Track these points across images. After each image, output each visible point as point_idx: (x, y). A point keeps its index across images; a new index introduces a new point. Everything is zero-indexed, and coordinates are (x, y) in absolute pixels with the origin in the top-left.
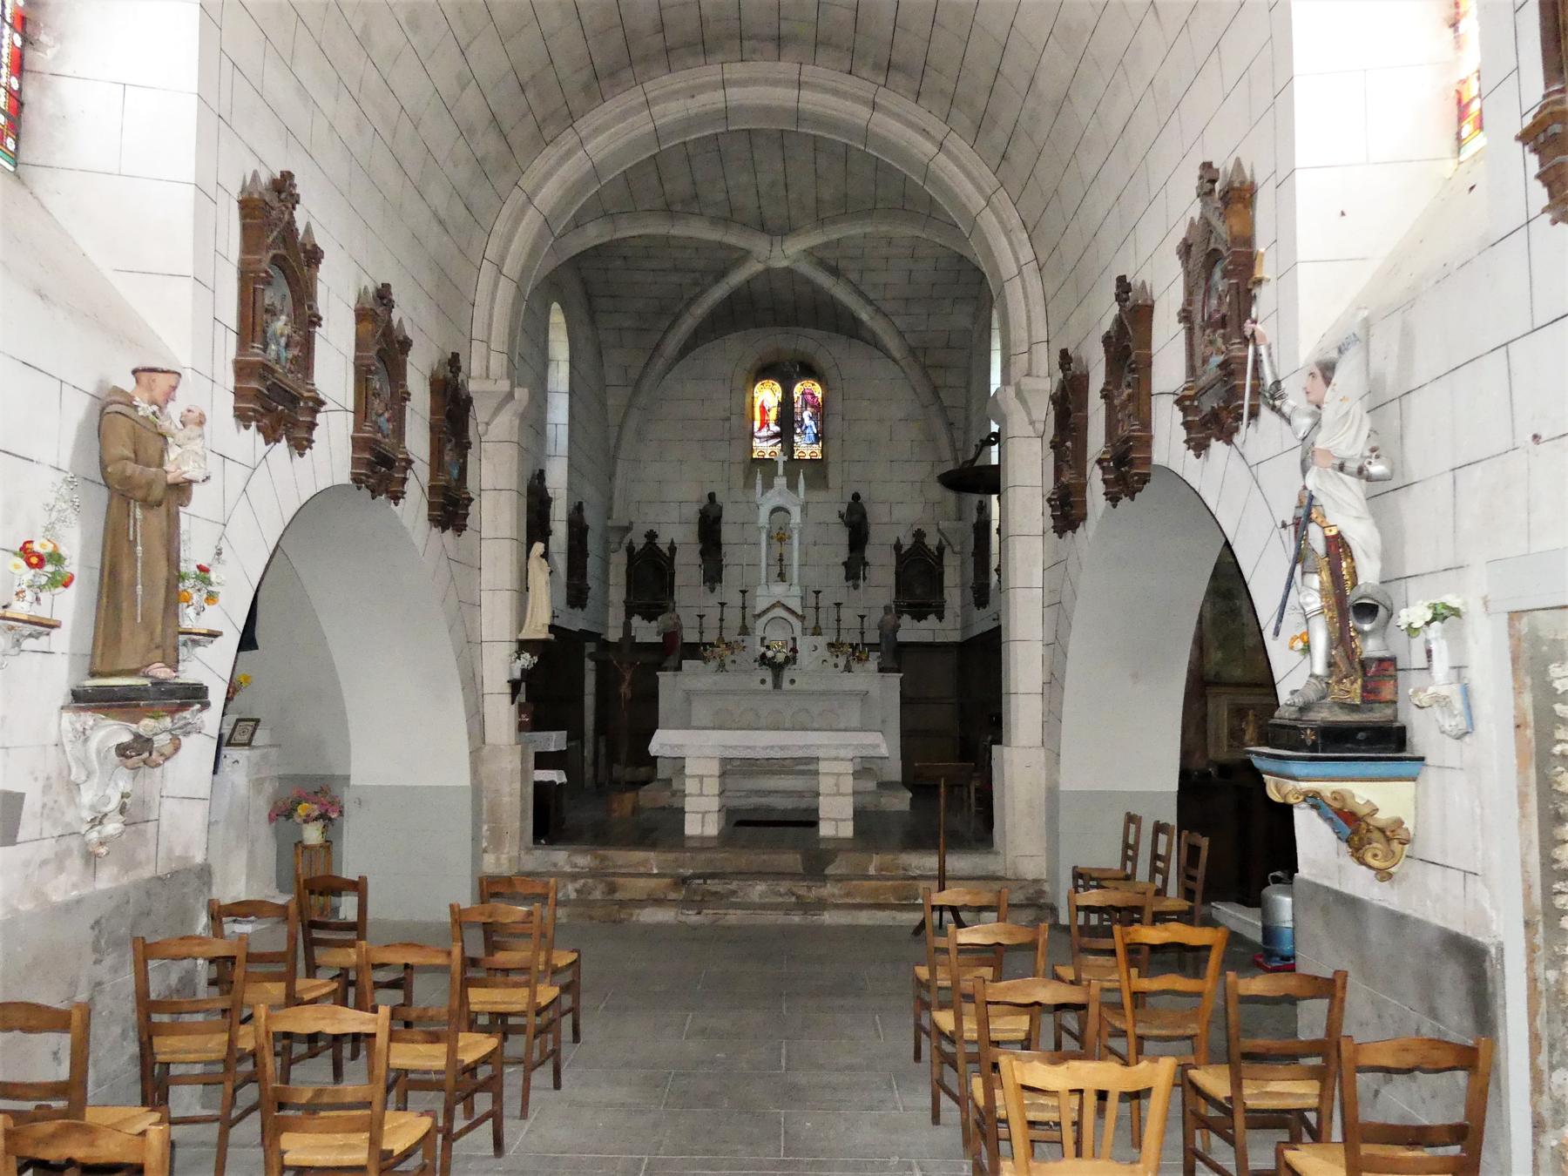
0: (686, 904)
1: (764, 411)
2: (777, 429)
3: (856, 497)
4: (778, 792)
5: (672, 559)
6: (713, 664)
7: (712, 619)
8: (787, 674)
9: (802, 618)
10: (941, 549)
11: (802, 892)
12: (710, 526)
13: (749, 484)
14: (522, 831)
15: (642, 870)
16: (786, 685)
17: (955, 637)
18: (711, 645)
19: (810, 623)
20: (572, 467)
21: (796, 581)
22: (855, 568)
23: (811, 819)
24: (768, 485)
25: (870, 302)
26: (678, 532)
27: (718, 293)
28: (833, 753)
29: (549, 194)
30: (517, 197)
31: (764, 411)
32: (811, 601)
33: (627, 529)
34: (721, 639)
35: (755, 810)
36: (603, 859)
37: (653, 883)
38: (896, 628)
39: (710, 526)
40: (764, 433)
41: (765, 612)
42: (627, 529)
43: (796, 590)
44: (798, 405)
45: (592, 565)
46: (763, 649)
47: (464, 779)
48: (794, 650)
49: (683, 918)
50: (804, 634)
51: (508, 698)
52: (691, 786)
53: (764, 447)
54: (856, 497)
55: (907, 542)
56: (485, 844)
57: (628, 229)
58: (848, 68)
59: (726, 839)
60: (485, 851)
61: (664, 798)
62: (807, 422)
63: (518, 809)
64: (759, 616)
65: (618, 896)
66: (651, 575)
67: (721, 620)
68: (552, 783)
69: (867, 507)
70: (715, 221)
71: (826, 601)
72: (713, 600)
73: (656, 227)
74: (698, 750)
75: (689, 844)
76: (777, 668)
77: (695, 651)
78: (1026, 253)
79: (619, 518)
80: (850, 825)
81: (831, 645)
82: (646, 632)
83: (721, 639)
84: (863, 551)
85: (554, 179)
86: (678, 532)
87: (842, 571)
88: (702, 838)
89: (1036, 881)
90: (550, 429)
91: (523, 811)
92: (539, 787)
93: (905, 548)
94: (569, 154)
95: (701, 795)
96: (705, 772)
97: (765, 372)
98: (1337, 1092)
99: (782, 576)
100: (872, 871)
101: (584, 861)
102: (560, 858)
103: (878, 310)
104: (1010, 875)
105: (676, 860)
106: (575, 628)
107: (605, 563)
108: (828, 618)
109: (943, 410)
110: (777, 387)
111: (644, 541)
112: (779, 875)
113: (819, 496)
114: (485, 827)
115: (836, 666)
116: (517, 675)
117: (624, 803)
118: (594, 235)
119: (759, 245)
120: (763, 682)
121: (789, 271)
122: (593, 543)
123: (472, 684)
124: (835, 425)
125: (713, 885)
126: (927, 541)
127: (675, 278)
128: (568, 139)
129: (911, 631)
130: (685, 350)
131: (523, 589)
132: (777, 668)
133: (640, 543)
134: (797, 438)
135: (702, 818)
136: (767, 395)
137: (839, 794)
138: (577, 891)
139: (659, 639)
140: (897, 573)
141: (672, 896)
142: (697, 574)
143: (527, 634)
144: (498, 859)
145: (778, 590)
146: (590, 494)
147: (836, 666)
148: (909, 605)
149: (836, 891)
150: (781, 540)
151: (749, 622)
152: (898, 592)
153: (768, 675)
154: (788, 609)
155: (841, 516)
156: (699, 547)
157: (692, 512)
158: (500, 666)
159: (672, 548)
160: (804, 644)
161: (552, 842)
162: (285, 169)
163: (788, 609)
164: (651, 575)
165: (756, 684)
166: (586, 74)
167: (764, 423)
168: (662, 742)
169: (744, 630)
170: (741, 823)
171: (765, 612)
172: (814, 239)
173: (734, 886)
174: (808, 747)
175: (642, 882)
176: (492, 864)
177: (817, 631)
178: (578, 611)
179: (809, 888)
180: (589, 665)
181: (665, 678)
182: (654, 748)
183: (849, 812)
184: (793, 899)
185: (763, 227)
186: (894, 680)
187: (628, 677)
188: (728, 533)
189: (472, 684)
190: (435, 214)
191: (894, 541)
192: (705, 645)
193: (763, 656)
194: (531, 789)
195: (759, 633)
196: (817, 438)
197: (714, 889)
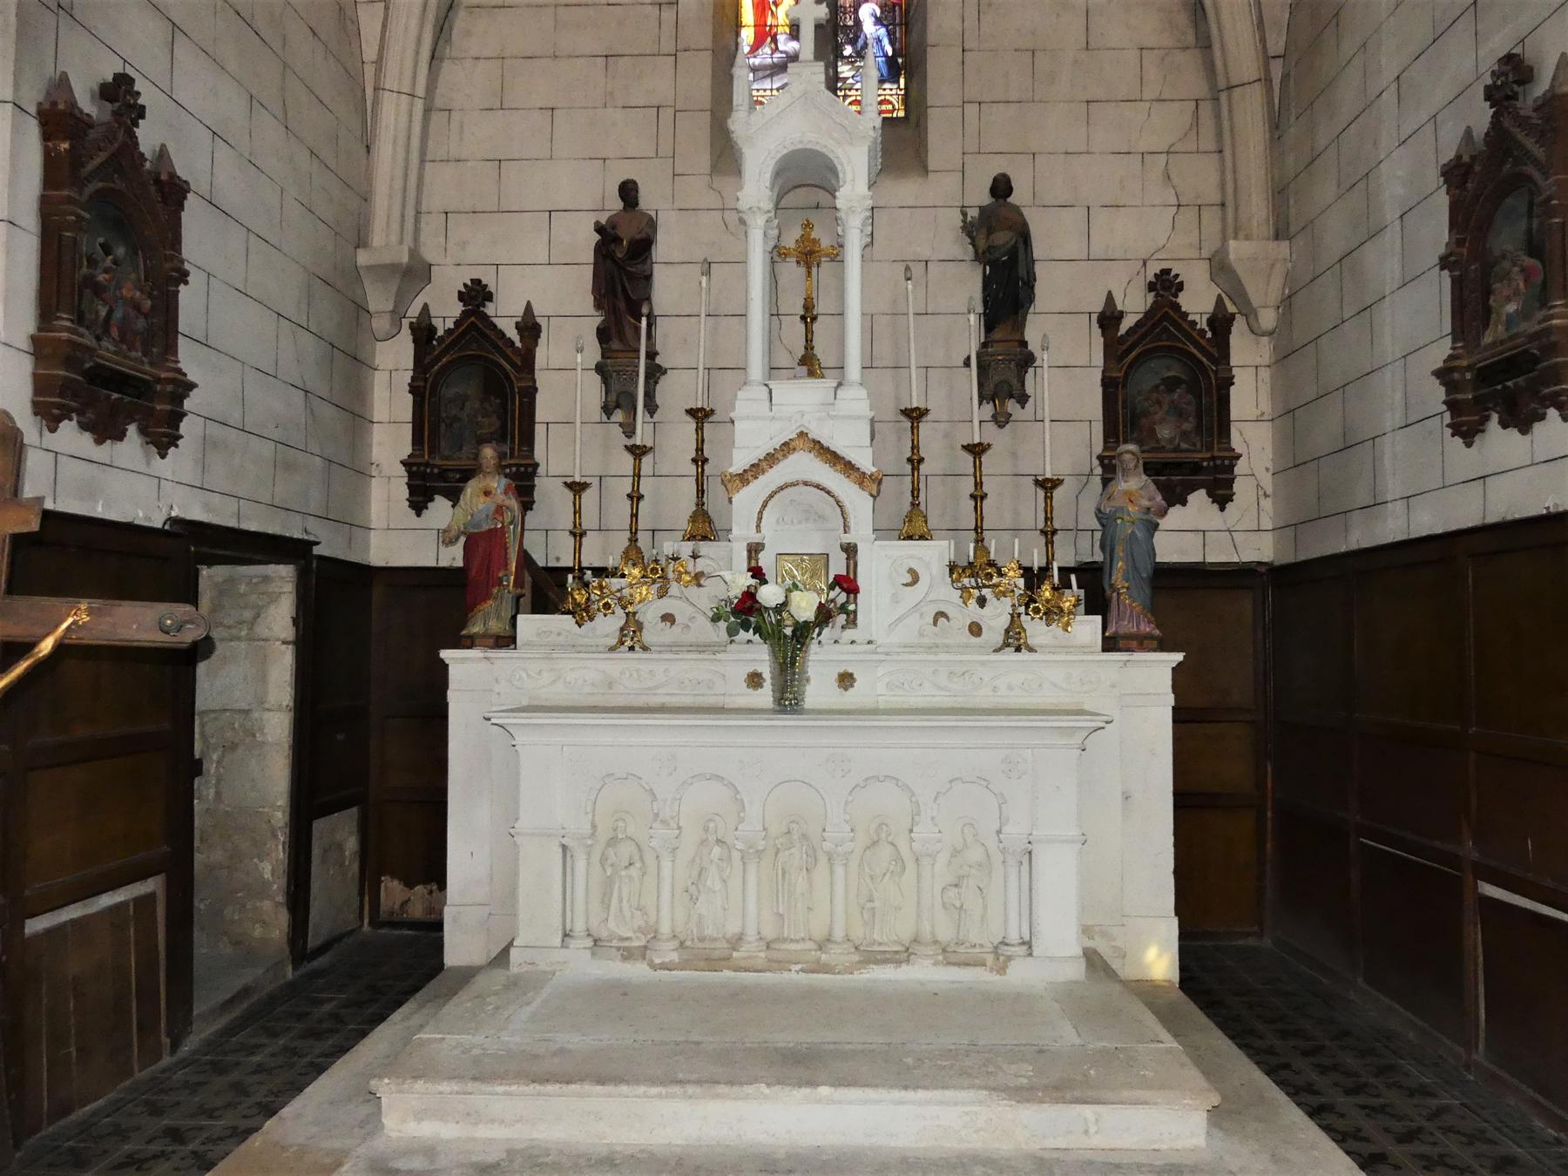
3: (1001, 187)
5: (526, 362)
6: (607, 626)
8: (822, 659)
10: (1221, 323)
12: (622, 265)
16: (818, 688)
17: (1261, 549)
22: (1003, 374)
26: (548, 286)
34: (633, 553)
39: (622, 265)
41: (756, 470)
43: (856, 401)
48: (847, 584)
50: (880, 532)
54: (1001, 187)
55: (1135, 305)
62: (870, 28)
64: (745, 478)
66: (475, 386)
76: (791, 644)
77: (548, 590)
79: (386, 242)
84: (1020, 326)
86: (548, 286)
93: (1127, 323)
98: (1241, 942)
99: (809, 364)
108: (946, 499)
111: (457, 309)
113: (906, 190)
115: (975, 629)
126: (1186, 301)
129: (1191, 533)
133: (447, 313)
139: (453, 556)
140: (1108, 384)
142: (592, 390)
145: (802, 401)
147: (975, 629)
150: (809, 255)
151: (713, 503)
153: (760, 656)
154: (832, 457)
159: (530, 328)
160: (881, 564)
162: (475, 277)
163: (832, 457)
164: (475, 386)
169: (704, 527)
171: (756, 470)
177: (913, 528)
186: (1155, 672)
188: (670, 287)
191: (1098, 306)
195: (742, 531)
196: (892, 70)
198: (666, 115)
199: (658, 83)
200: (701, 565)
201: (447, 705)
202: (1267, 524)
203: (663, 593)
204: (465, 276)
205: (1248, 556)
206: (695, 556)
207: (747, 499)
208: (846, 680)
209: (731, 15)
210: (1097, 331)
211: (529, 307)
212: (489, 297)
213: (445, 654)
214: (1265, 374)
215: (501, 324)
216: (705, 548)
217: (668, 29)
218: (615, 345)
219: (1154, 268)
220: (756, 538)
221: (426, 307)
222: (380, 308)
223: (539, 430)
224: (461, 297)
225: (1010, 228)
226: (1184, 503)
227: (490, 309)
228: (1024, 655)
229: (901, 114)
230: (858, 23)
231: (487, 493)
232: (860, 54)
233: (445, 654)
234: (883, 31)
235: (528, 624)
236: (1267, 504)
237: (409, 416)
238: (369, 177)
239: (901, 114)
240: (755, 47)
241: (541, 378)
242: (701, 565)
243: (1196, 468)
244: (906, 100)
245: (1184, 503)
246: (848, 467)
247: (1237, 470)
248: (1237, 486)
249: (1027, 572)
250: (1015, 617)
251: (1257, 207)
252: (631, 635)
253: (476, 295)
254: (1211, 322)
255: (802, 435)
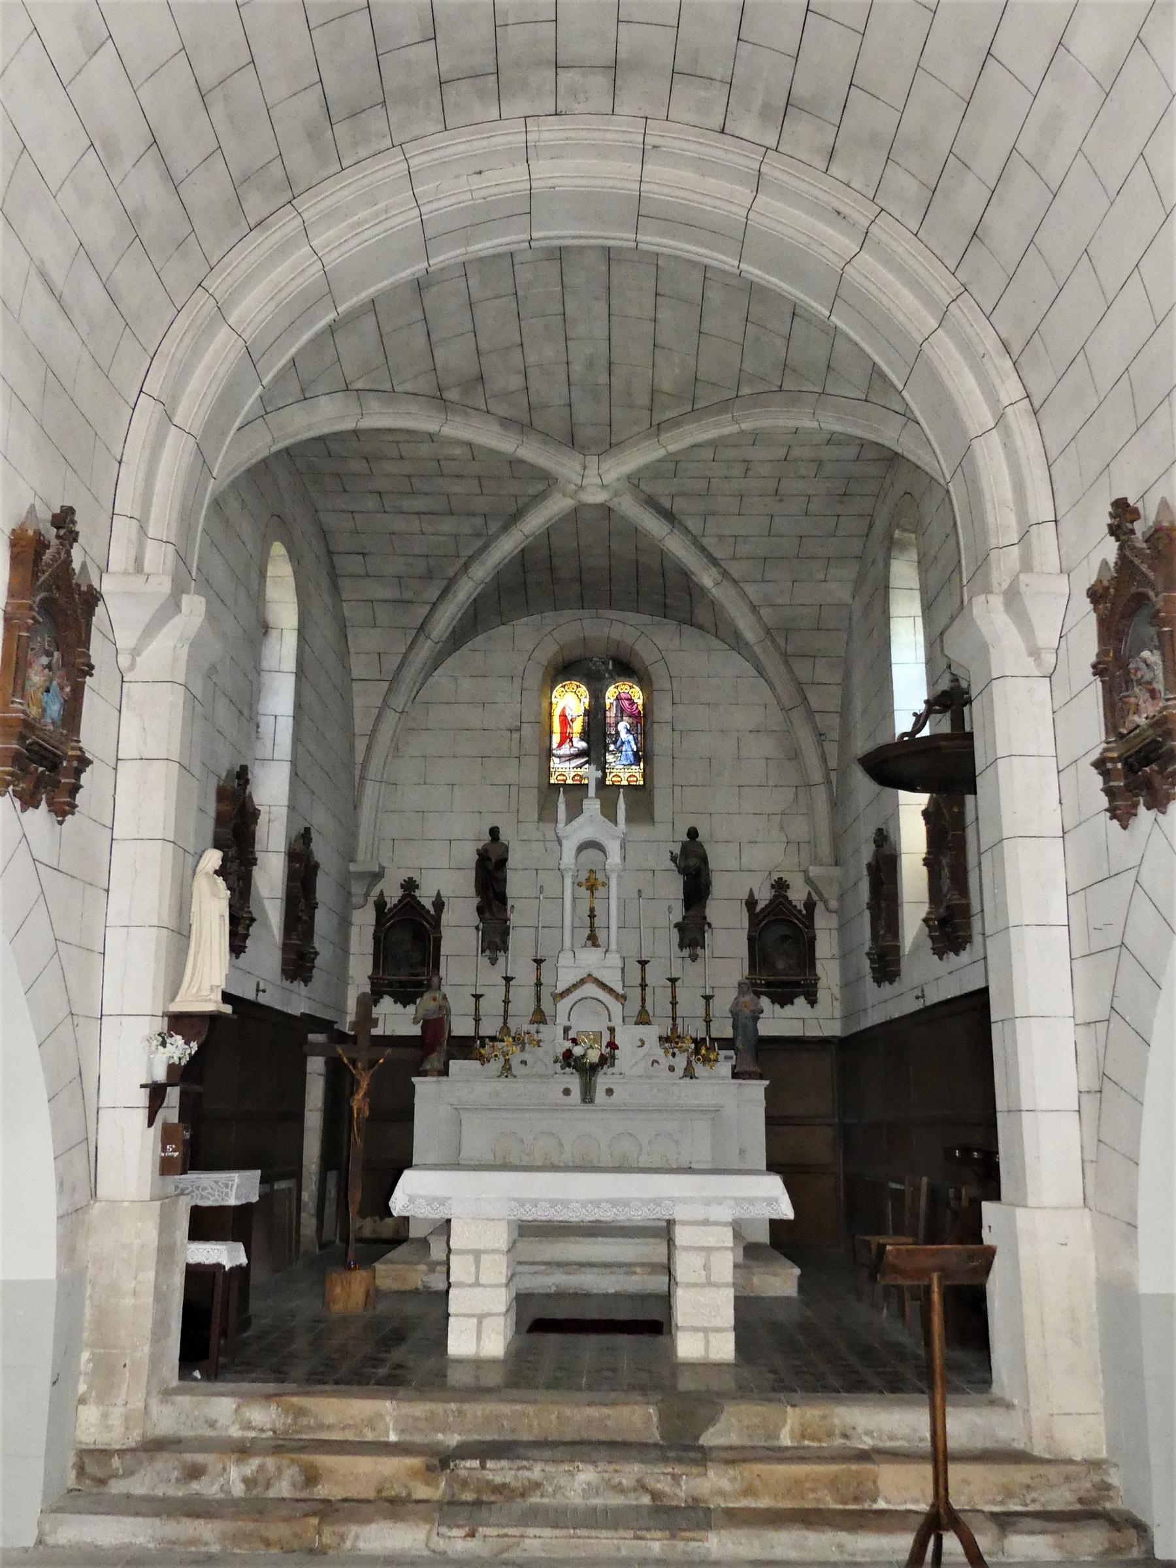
0: (448, 1511)
1: (565, 721)
2: (583, 745)
3: (693, 833)
4: (602, 1275)
6: (495, 1066)
7: (492, 1004)
8: (602, 1081)
9: (622, 998)
10: (810, 906)
11: (663, 1485)
12: (491, 872)
13: (546, 812)
14: (155, 1361)
15: (370, 1436)
17: (834, 1029)
18: (493, 1039)
19: (634, 1006)
20: (295, 776)
21: (613, 946)
22: (692, 934)
23: (655, 1315)
24: (575, 811)
25: (715, 562)
26: (449, 882)
27: (507, 546)
28: (699, 1213)
29: (253, 308)
30: (202, 305)
31: (565, 721)
32: (635, 978)
33: (377, 876)
34: (505, 1028)
35: (560, 1296)
36: (300, 1412)
37: (390, 1466)
38: (756, 1015)
39: (491, 872)
40: (566, 750)
41: (568, 991)
42: (377, 876)
43: (614, 959)
44: (611, 714)
45: (323, 921)
46: (568, 1044)
47: (43, 1264)
48: (612, 1045)
49: (440, 1544)
51: (142, 1115)
52: (460, 1269)
53: (564, 770)
54: (693, 833)
55: (764, 896)
56: (82, 1388)
57: (378, 417)
58: (717, 123)
59: (519, 1373)
60: (82, 1401)
61: (419, 1277)
62: (624, 736)
63: (147, 1322)
64: (563, 995)
65: (322, 1491)
66: (408, 940)
67: (506, 1002)
68: (219, 1266)
69: (707, 847)
70: (506, 423)
71: (656, 976)
72: (494, 976)
73: (420, 420)
74: (477, 1208)
75: (456, 1377)
76: (588, 1071)
77: (467, 1047)
78: (1010, 390)
79: (364, 862)
80: (731, 1337)
81: (663, 1040)
82: (396, 1020)
83: (505, 1028)
85: (267, 284)
86: (449, 882)
87: (675, 936)
88: (478, 1364)
89: (1095, 1465)
90: (266, 724)
91: (160, 1324)
92: (197, 1276)
93: (758, 909)
94: (283, 250)
95: (477, 1284)
96: (482, 1247)
97: (566, 669)
100: (786, 1440)
101: (263, 1417)
102: (229, 1411)
103: (725, 574)
104: (1039, 1450)
105: (430, 1418)
106: (297, 1013)
107: (345, 923)
108: (659, 1003)
109: (810, 713)
110: (583, 689)
111: (400, 893)
112: (618, 1448)
113: (643, 832)
114: (85, 1355)
115: (672, 1069)
116: (160, 1075)
117: (349, 1292)
118: (328, 416)
119: (565, 466)
120: (567, 1092)
121: (606, 510)
122: (325, 889)
123: (73, 1090)
124: (662, 740)
125: (500, 1471)
127: (448, 525)
128: (286, 226)
129: (779, 1021)
130: (458, 638)
131: (181, 933)
132: (586, 1069)
133: (394, 896)
134: (610, 758)
135: (478, 1329)
136: (571, 701)
137: (710, 1284)
138: (246, 1481)
139: (416, 1031)
140: (751, 939)
141: (422, 1492)
143: (185, 1003)
144: (105, 1416)
145: (590, 959)
146: (320, 819)
147: (672, 1069)
148: (769, 984)
149: (725, 1484)
150: (592, 888)
152: (752, 966)
153: (574, 1082)
155: (673, 859)
156: (476, 901)
157: (468, 855)
158: (134, 1056)
159: (439, 904)
161: (212, 1375)
164: (408, 940)
165: (555, 1093)
166: (310, 103)
167: (566, 738)
168: (413, 1195)
169: (539, 1017)
170: (541, 1326)
171: (568, 991)
172: (640, 456)
173: (536, 1472)
174: (658, 1202)
175: (364, 1465)
176: (93, 1425)
177: (643, 1019)
178: (299, 986)
179: (676, 1478)
180: (316, 1065)
181: (424, 1086)
182: (399, 1203)
183: (727, 1316)
184: (646, 1500)
185: (572, 441)
186: (756, 1090)
187: (364, 1085)
188: (516, 884)
189: (73, 1090)
190: (43, 275)
192: (482, 1039)
193: (568, 1054)
194: (178, 1281)
195: (562, 1020)
196: (637, 758)
197: (498, 1479)
198: (514, 789)
199: (510, 773)
200: (541, 1036)
201: (413, 1105)
202: (838, 1014)
203: (523, 1049)
204: (405, 875)
205: (827, 1033)
206: (538, 1032)
207: (565, 1004)
208: (610, 1092)
209: (547, 728)
210: (745, 909)
211: (439, 894)
212: (417, 887)
213: (413, 1079)
214: (835, 933)
215: (423, 901)
216: (542, 1027)
217: (515, 744)
218: (487, 915)
219: (775, 877)
220: (568, 1024)
221: (382, 893)
222: (359, 892)
223: (443, 959)
224: (402, 886)
225: (454, 1389)
226: (792, 1003)
227: (417, 893)
228: (694, 1080)
229: (641, 783)
230: (618, 733)
231: (435, 999)
232: (619, 750)
233: (413, 1079)
234: (631, 737)
235: (454, 1065)
236: (837, 1004)
237: (372, 951)
238: (357, 826)
239: (641, 783)
240: (560, 746)
241: (445, 932)
242: (541, 1036)
243: (797, 984)
244: (644, 776)
245: (792, 1003)
246: (610, 991)
247: (819, 985)
248: (819, 995)
249: (695, 1041)
250: (689, 1063)
251: (825, 850)
252: (507, 1070)
253: (410, 886)
254: (805, 905)
255: (589, 975)
